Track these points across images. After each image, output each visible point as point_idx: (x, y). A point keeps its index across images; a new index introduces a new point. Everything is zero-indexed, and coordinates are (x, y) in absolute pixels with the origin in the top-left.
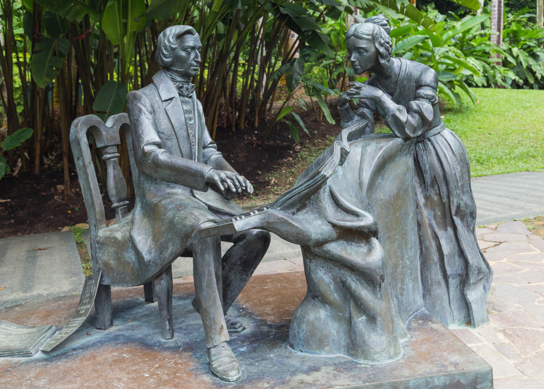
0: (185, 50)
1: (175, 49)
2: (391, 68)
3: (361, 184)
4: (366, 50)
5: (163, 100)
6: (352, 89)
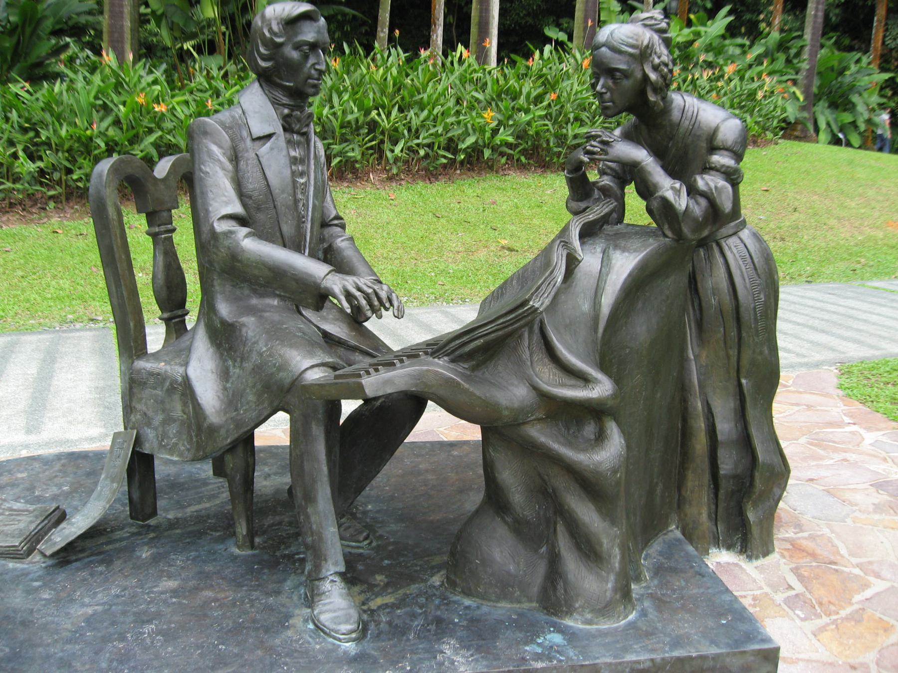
0: (298, 47)
1: (281, 45)
2: (666, 110)
3: (596, 318)
5: (254, 137)
6: (593, 143)
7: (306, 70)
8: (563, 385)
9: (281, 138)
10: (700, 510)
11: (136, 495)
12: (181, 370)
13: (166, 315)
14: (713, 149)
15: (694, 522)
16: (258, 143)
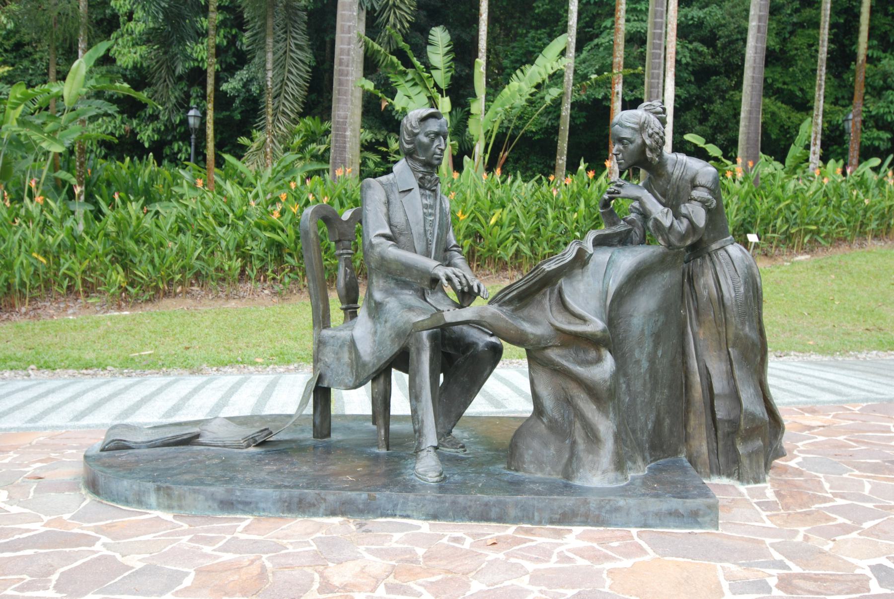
0: (427, 135)
1: (417, 134)
4: (631, 141)
7: (433, 149)
8: (570, 323)
9: (417, 190)
10: (701, 444)
11: (318, 421)
12: (349, 333)
13: (344, 307)
14: (694, 187)
15: (697, 452)
16: (402, 194)
